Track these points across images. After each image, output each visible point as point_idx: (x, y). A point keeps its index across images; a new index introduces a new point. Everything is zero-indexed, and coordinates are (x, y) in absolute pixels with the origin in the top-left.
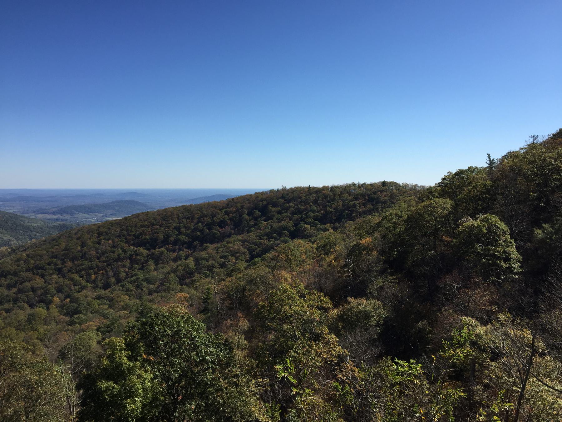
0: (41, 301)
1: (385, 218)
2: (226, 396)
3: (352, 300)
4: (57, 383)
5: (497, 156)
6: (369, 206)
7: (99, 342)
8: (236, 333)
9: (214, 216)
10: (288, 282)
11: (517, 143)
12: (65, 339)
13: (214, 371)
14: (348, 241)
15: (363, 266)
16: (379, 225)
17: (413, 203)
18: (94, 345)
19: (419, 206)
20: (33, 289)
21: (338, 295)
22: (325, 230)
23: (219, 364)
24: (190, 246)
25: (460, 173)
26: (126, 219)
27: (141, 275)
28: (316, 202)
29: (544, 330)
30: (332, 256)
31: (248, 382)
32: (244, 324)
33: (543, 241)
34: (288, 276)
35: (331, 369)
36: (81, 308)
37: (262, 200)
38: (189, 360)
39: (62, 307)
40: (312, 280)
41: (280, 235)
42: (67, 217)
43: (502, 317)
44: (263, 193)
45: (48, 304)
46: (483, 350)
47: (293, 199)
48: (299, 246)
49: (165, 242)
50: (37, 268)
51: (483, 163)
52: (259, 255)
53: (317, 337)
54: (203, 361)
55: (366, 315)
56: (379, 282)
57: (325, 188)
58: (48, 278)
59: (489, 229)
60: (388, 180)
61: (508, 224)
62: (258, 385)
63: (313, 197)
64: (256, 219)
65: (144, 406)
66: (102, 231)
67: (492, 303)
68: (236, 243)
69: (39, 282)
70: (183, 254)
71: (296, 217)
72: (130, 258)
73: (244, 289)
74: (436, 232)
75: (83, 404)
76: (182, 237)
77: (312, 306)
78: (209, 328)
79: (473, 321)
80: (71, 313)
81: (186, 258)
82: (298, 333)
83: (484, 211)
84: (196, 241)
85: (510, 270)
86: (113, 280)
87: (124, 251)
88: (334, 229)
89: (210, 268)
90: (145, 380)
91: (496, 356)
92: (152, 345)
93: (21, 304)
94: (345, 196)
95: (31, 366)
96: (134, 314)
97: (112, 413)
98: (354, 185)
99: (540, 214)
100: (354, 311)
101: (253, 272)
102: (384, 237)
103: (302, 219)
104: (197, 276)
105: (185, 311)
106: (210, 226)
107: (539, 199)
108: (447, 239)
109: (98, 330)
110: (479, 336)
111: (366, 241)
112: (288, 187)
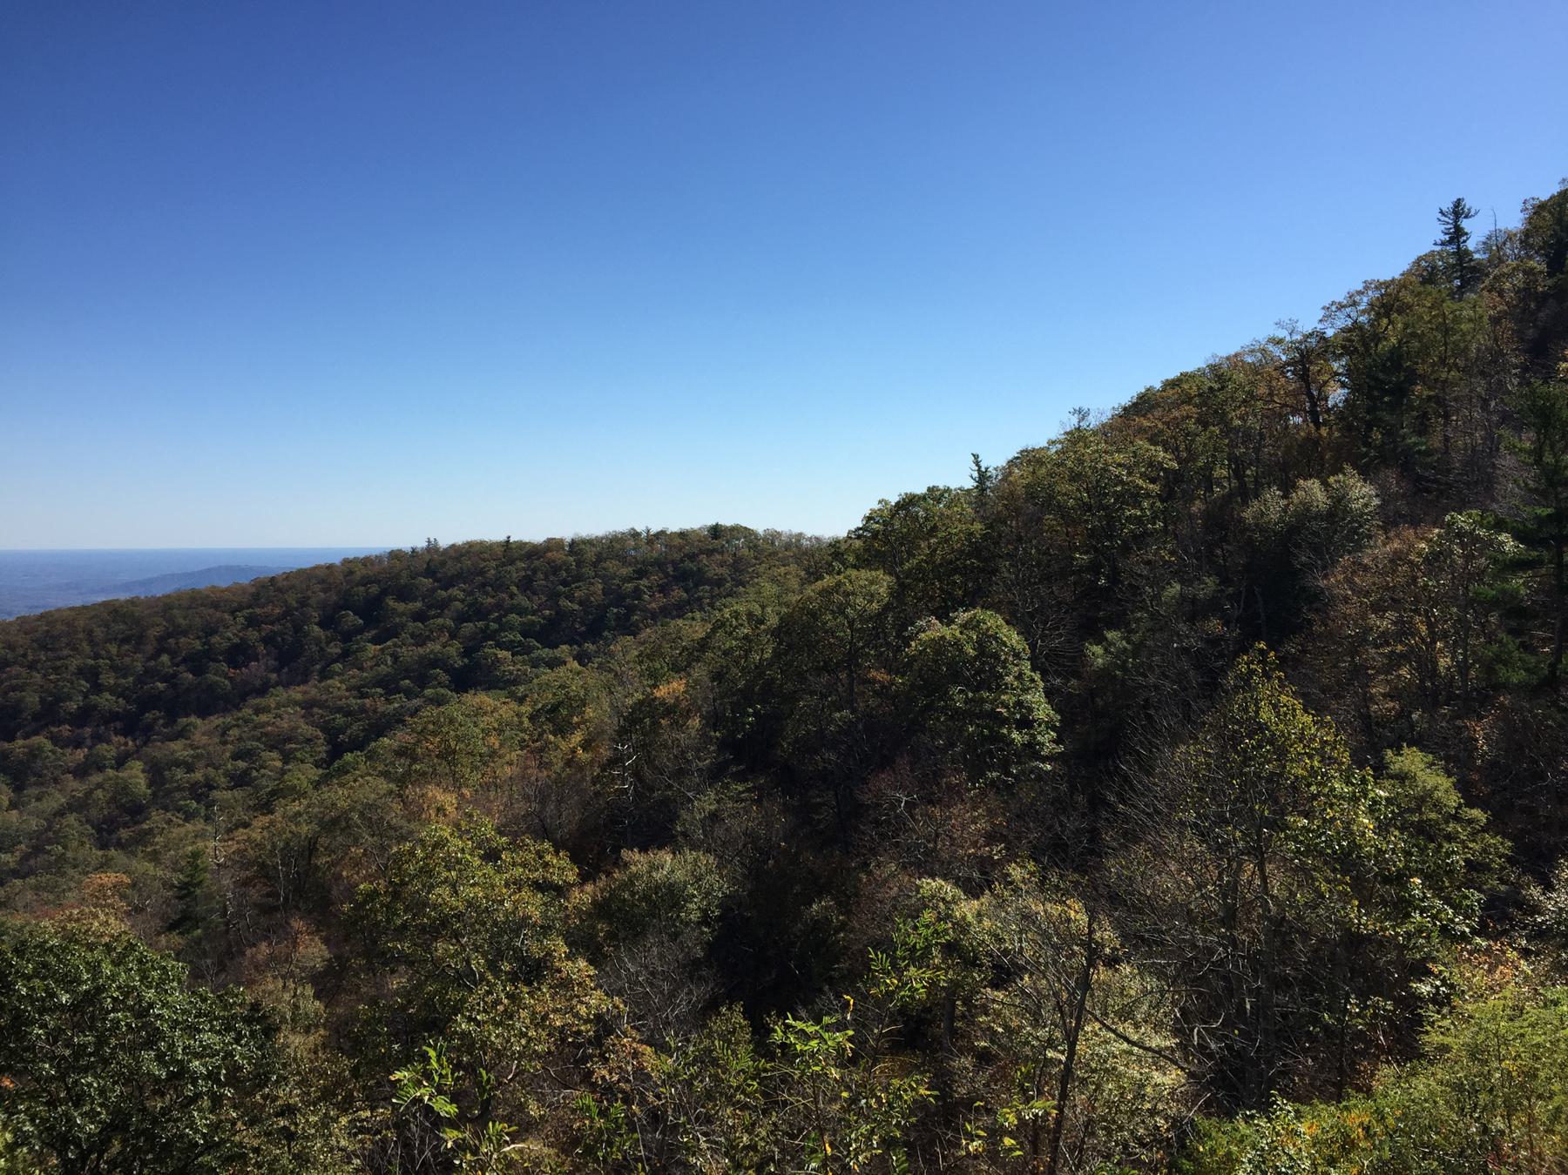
1: (720, 625)
5: (996, 459)
6: (678, 594)
8: (288, 987)
9: (210, 631)
13: (217, 1101)
15: (664, 759)
16: (703, 645)
17: (794, 583)
19: (809, 591)
21: (594, 847)
22: (553, 664)
23: (234, 1079)
24: (131, 725)
25: (908, 502)
28: (526, 585)
29: (1114, 899)
30: (577, 738)
31: (326, 1122)
32: (313, 952)
33: (1105, 674)
34: (448, 800)
35: (574, 1056)
38: (131, 1077)
40: (520, 808)
41: (422, 681)
43: (1016, 872)
44: (367, 561)
46: (972, 962)
48: (479, 711)
49: (48, 716)
51: (961, 479)
52: (357, 745)
53: (533, 971)
54: (181, 1074)
55: (672, 896)
56: (707, 802)
57: (552, 545)
59: (981, 646)
60: (727, 521)
61: (1026, 633)
62: (356, 1129)
63: (516, 571)
64: (347, 637)
67: (991, 838)
68: (284, 708)
70: (107, 750)
73: (311, 848)
74: (853, 657)
76: (106, 700)
77: (518, 884)
78: (197, 975)
79: (949, 890)
81: (120, 762)
82: (478, 963)
84: (150, 710)
85: (1032, 749)
88: (582, 658)
89: (200, 793)
91: (1003, 975)
94: (611, 566)
98: (635, 535)
99: (1098, 606)
100: (640, 886)
101: (338, 796)
102: (718, 676)
104: (157, 817)
105: (116, 926)
106: (197, 663)
107: (1094, 568)
108: (881, 676)
110: (962, 927)
111: (671, 689)
112: (444, 542)
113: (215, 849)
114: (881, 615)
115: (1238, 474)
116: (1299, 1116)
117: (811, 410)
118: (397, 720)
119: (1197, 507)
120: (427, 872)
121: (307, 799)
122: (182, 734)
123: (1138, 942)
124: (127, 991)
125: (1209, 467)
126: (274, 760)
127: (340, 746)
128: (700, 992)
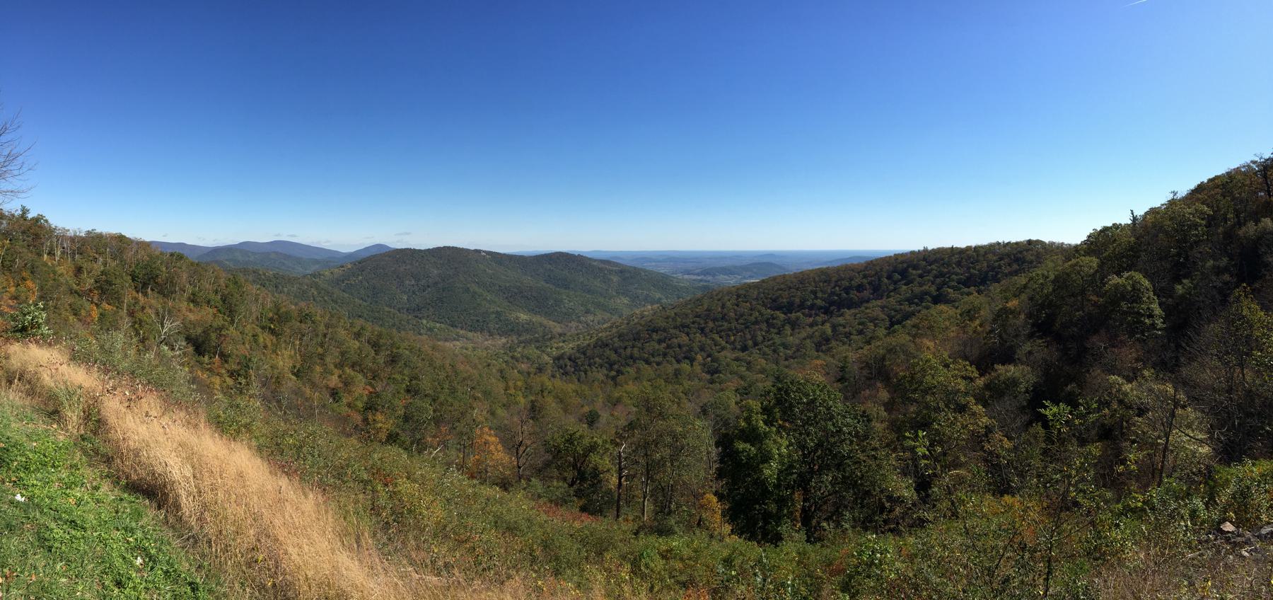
0: (686, 358)
1: (1031, 279)
2: (864, 470)
3: (999, 367)
4: (698, 437)
5: (1140, 212)
6: (1015, 266)
7: (737, 403)
8: (876, 403)
9: (851, 279)
10: (931, 351)
11: (1156, 198)
12: (707, 397)
13: (852, 442)
14: (993, 305)
15: (1010, 330)
16: (1025, 287)
17: (1060, 262)
18: (733, 405)
19: (1066, 265)
20: (680, 346)
21: (984, 363)
22: (969, 294)
23: (857, 435)
24: (827, 311)
25: (1105, 229)
26: (763, 281)
27: (777, 340)
28: (959, 264)
29: (1185, 384)
30: (978, 322)
31: (887, 455)
32: (884, 395)
33: (1182, 296)
34: (931, 344)
35: (978, 440)
36: (721, 368)
37: (902, 262)
38: (825, 430)
39: (704, 365)
40: (956, 348)
41: (922, 300)
42: (710, 278)
43: (1146, 373)
44: (902, 255)
45: (692, 360)
46: (1129, 407)
47: (935, 261)
48: (942, 312)
49: (802, 306)
50: (683, 326)
51: (1126, 220)
52: (899, 322)
53: (962, 409)
54: (840, 431)
55: (1014, 382)
56: (1027, 347)
57: (969, 248)
58: (692, 336)
59: (1133, 286)
60: (1034, 238)
61: (1151, 281)
62: (898, 459)
63: (955, 259)
64: (895, 283)
65: (780, 472)
66: (741, 294)
67: (1137, 360)
68: (875, 308)
69: (684, 339)
70: (819, 319)
71: (938, 280)
72: (767, 321)
73: (883, 359)
74: (1083, 292)
75: (721, 461)
76: (819, 302)
77: (955, 377)
78: (846, 398)
79: (1120, 380)
80: (712, 372)
81: (823, 324)
82: (942, 405)
83: (1129, 269)
84: (833, 306)
85: (1153, 326)
86: (750, 343)
87: (761, 314)
88: (979, 292)
89: (848, 335)
90: (781, 446)
91: (1141, 412)
92: (787, 412)
93: (669, 358)
94: (990, 256)
95: (677, 417)
96: (772, 379)
97: (749, 475)
98: (999, 244)
99: (1180, 270)
100: (1002, 378)
101: (892, 340)
102: (1031, 299)
103: (944, 283)
104: (834, 343)
105: (821, 379)
106: (847, 290)
107: (1179, 255)
108: (1094, 298)
109: (736, 390)
110: (1126, 394)
111: (1013, 304)
112: (930, 248)
113: (852, 356)
114: (1094, 275)
115: (1237, 216)
116: (1254, 465)
117: (1067, 198)
118: (913, 314)
119: (1220, 230)
120: (923, 370)
121: (883, 341)
122: (842, 315)
123: (1195, 400)
124: (824, 401)
125: (1225, 214)
126: (871, 326)
127: (894, 322)
128: (1026, 418)
